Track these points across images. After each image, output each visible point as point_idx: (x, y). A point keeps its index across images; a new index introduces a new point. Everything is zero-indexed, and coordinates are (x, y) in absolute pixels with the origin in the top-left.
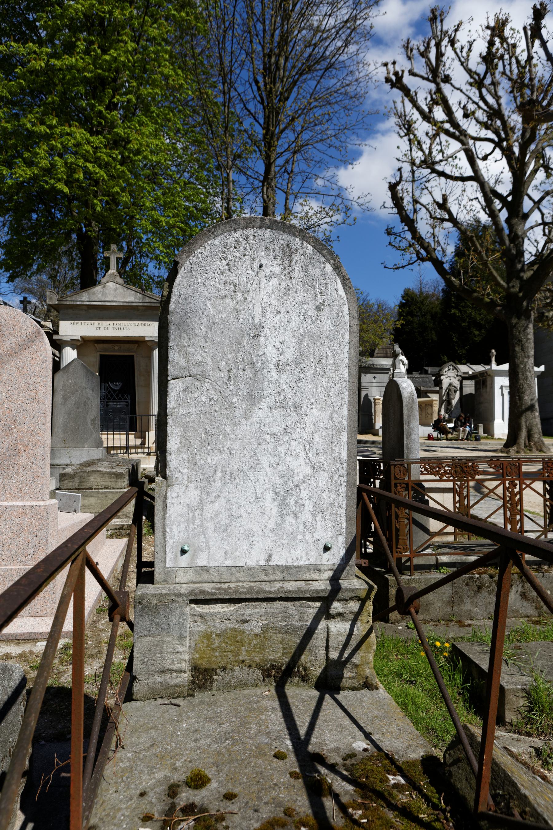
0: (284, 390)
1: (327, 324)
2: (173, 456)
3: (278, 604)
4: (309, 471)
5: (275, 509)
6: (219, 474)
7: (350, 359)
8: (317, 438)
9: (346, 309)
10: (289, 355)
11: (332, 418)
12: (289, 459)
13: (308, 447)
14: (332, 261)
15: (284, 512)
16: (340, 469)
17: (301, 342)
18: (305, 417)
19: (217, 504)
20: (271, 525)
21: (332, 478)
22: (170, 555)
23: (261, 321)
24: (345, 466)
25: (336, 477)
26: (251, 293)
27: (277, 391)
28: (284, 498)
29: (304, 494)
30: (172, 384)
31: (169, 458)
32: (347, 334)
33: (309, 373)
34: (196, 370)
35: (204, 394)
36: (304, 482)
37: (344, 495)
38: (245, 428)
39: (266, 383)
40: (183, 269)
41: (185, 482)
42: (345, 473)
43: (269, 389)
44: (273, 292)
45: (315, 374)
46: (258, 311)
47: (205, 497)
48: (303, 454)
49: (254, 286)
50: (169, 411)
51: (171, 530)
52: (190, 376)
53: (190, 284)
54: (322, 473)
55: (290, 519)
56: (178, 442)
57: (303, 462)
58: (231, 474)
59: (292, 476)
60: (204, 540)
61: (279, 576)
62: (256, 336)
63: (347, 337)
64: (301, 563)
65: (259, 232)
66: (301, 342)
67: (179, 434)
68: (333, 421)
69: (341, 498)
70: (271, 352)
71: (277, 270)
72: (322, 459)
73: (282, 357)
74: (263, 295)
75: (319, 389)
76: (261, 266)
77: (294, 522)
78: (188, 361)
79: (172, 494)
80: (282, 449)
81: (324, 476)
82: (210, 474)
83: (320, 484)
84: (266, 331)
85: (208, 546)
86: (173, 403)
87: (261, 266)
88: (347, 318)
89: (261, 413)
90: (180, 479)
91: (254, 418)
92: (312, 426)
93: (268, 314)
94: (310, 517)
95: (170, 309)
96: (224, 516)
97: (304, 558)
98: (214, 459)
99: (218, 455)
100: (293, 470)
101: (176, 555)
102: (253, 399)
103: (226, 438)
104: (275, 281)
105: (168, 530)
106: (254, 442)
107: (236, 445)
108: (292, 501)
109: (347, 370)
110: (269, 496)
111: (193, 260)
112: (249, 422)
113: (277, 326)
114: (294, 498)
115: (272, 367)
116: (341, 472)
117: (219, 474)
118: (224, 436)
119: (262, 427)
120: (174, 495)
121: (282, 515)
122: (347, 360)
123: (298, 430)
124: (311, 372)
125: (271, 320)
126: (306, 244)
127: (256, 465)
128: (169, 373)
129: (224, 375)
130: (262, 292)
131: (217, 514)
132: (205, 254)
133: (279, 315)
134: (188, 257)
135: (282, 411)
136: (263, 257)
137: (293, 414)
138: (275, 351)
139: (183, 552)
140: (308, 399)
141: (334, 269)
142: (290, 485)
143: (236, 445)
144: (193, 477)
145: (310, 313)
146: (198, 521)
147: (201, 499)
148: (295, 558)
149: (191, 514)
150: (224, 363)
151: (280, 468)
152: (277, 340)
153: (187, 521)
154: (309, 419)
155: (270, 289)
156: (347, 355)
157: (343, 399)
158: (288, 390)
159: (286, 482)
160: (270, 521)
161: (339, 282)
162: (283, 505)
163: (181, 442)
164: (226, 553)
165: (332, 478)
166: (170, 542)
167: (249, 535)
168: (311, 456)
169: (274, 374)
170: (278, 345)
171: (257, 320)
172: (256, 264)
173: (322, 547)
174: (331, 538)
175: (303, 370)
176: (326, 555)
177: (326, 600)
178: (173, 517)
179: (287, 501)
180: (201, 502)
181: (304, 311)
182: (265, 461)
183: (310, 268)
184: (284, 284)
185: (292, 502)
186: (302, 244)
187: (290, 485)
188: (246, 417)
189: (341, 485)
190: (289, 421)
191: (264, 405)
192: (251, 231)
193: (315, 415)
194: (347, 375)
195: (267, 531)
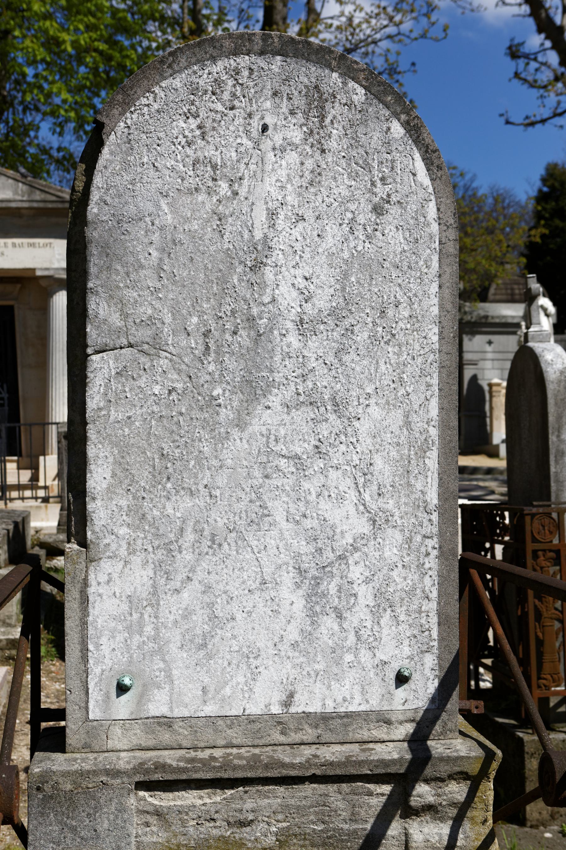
1: (394, 240)
3: (309, 789)
10: (322, 301)
12: (324, 505)
20: (293, 634)
34: (141, 334)
38: (238, 446)
43: (284, 369)
53: (126, 165)
55: (329, 623)
61: (309, 734)
62: (257, 267)
65: (261, 62)
70: (288, 297)
71: (296, 135)
74: (269, 186)
80: (311, 486)
84: (278, 257)
89: (269, 417)
91: (256, 427)
102: (253, 390)
104: (293, 157)
111: (132, 118)
121: (313, 615)
125: (287, 234)
129: (195, 343)
136: (269, 111)
139: (122, 689)
154: (363, 427)
167: (250, 655)
176: (401, 693)
177: (402, 780)
182: (278, 510)
188: (241, 425)
192: (244, 61)
193: (374, 417)
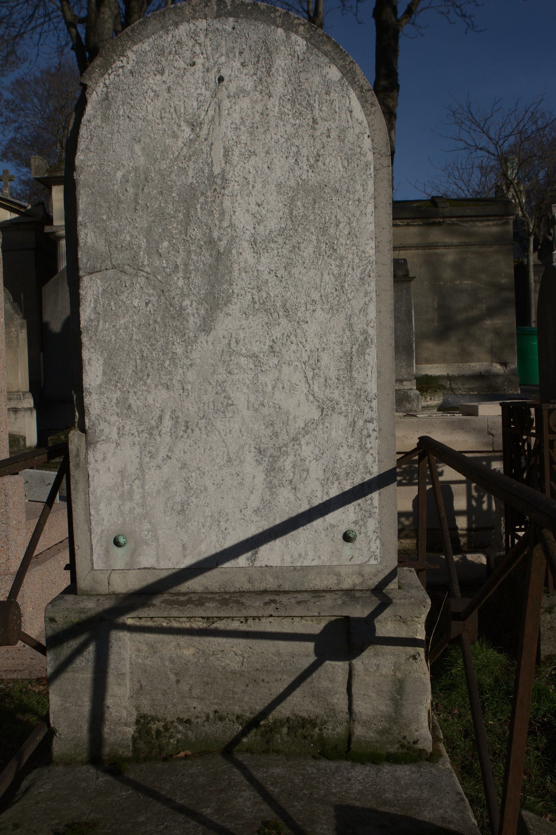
0: (267, 282)
1: (335, 167)
2: (94, 396)
4: (316, 415)
5: (261, 477)
6: (167, 423)
7: (377, 225)
8: (325, 358)
9: (367, 143)
11: (350, 326)
12: (279, 395)
13: (310, 375)
14: (341, 62)
15: (275, 481)
16: (367, 410)
17: (292, 200)
18: (305, 326)
19: (165, 469)
21: (354, 424)
22: (98, 550)
23: (223, 171)
24: (374, 404)
25: (361, 423)
26: (205, 127)
27: (254, 283)
28: (274, 459)
29: (307, 451)
30: (86, 282)
31: (87, 400)
32: (371, 183)
33: (308, 251)
34: (120, 257)
35: (138, 298)
36: (307, 433)
37: (374, 452)
38: (205, 348)
39: (236, 274)
40: (94, 95)
41: (114, 436)
42: (374, 415)
44: (243, 122)
45: (318, 252)
46: (218, 153)
47: (147, 459)
48: (304, 388)
49: (211, 113)
50: (83, 324)
51: (97, 510)
52: (114, 267)
54: (335, 416)
56: (100, 373)
57: (303, 398)
58: (187, 422)
59: (286, 423)
60: (149, 527)
63: (371, 188)
64: (306, 563)
65: (217, 24)
66: (292, 200)
67: (101, 362)
68: (352, 330)
69: (369, 459)
70: (243, 220)
71: (249, 84)
72: (336, 395)
73: (261, 229)
75: (326, 278)
76: (221, 79)
77: (292, 497)
78: (109, 243)
79: (95, 459)
80: (267, 379)
81: (338, 426)
82: (153, 423)
83: (334, 434)
85: (156, 538)
86: (88, 311)
87: (221, 79)
88: (370, 157)
89: (228, 323)
90: (107, 431)
92: (316, 341)
93: (235, 158)
94: (320, 489)
95: (77, 163)
96: (178, 487)
97: (311, 554)
98: (159, 397)
99: (164, 392)
100: (287, 413)
101: (107, 551)
102: (215, 303)
103: (175, 365)
104: (245, 103)
105: (92, 512)
106: (221, 370)
107: (191, 376)
108: (287, 463)
109: (373, 244)
110: (250, 457)
111: (109, 78)
112: (210, 338)
113: (250, 178)
114: (291, 458)
115: (245, 245)
116: (369, 415)
117: (167, 423)
118: (172, 359)
119: (233, 345)
120: (99, 456)
121: (271, 487)
122: (372, 227)
123: (294, 347)
124: (311, 250)
126: (294, 37)
127: (227, 405)
128: (81, 265)
130: (224, 123)
131: (167, 484)
132: (129, 67)
133: (253, 159)
134: (103, 75)
135: (262, 318)
137: (284, 321)
138: (249, 217)
140: (308, 295)
141: (344, 75)
142: (284, 437)
143: (191, 376)
144: (127, 428)
145: (304, 152)
146: (137, 497)
147: (141, 464)
148: (296, 555)
149: (126, 487)
150: (166, 244)
151: (265, 411)
152: (252, 200)
153: (121, 497)
154: (312, 329)
155: (236, 116)
156: (372, 219)
157: (366, 294)
158: (272, 280)
159: (276, 434)
160: (252, 497)
161: (353, 95)
162: (272, 470)
163: (104, 373)
164: (184, 547)
165: (354, 424)
166: (97, 530)
168: (316, 389)
169: (248, 256)
170: (254, 208)
171: (217, 170)
172: (213, 76)
173: (340, 536)
174: (356, 523)
175: (296, 248)
178: (98, 491)
179: (279, 464)
180: (141, 467)
181: (294, 149)
182: (240, 398)
183: (303, 76)
184: (259, 107)
185: (288, 465)
186: (288, 37)
187: (284, 437)
188: (206, 327)
189: (369, 436)
190: (277, 332)
191: (234, 308)
194: (372, 252)
195: (248, 512)
